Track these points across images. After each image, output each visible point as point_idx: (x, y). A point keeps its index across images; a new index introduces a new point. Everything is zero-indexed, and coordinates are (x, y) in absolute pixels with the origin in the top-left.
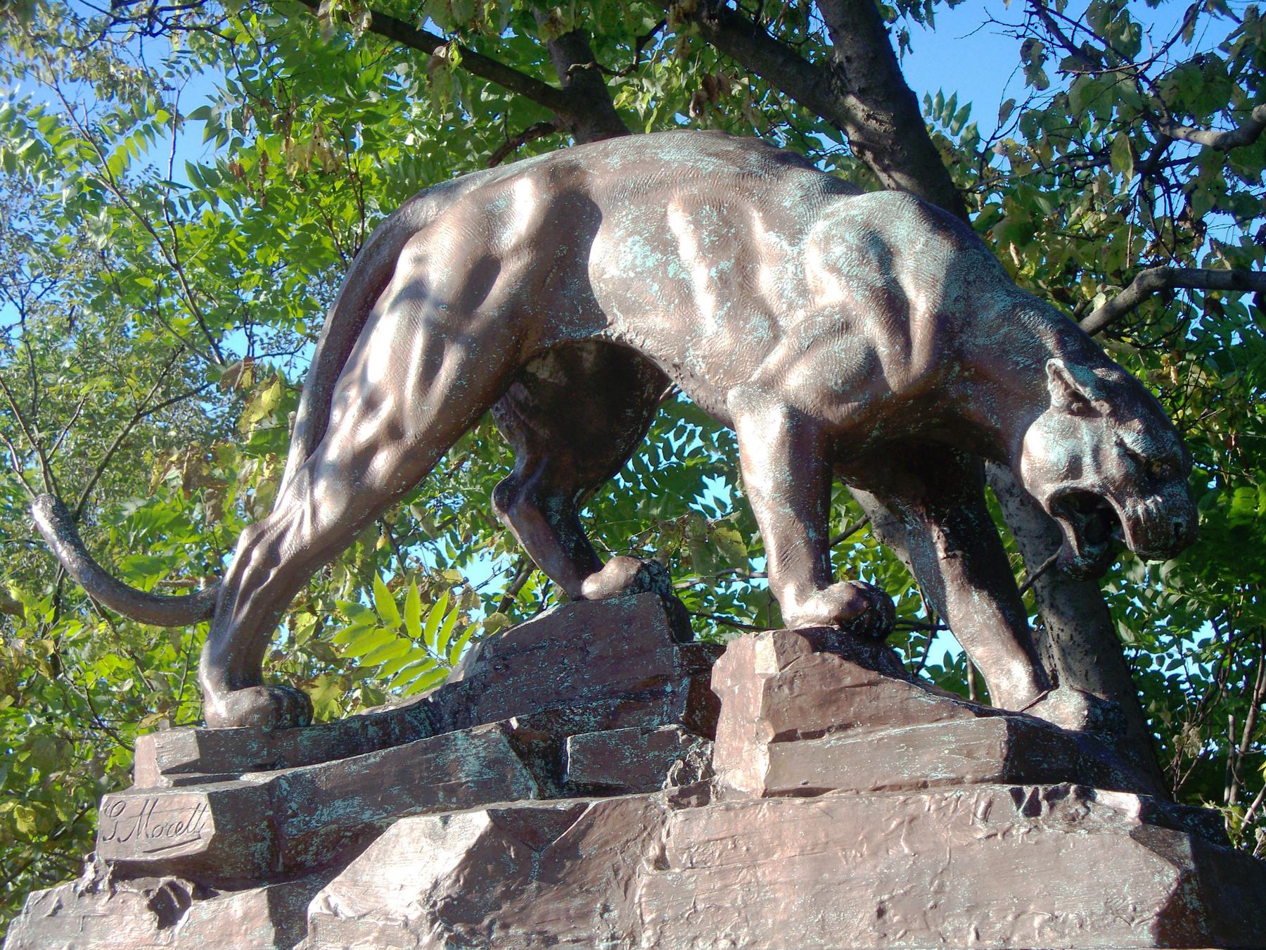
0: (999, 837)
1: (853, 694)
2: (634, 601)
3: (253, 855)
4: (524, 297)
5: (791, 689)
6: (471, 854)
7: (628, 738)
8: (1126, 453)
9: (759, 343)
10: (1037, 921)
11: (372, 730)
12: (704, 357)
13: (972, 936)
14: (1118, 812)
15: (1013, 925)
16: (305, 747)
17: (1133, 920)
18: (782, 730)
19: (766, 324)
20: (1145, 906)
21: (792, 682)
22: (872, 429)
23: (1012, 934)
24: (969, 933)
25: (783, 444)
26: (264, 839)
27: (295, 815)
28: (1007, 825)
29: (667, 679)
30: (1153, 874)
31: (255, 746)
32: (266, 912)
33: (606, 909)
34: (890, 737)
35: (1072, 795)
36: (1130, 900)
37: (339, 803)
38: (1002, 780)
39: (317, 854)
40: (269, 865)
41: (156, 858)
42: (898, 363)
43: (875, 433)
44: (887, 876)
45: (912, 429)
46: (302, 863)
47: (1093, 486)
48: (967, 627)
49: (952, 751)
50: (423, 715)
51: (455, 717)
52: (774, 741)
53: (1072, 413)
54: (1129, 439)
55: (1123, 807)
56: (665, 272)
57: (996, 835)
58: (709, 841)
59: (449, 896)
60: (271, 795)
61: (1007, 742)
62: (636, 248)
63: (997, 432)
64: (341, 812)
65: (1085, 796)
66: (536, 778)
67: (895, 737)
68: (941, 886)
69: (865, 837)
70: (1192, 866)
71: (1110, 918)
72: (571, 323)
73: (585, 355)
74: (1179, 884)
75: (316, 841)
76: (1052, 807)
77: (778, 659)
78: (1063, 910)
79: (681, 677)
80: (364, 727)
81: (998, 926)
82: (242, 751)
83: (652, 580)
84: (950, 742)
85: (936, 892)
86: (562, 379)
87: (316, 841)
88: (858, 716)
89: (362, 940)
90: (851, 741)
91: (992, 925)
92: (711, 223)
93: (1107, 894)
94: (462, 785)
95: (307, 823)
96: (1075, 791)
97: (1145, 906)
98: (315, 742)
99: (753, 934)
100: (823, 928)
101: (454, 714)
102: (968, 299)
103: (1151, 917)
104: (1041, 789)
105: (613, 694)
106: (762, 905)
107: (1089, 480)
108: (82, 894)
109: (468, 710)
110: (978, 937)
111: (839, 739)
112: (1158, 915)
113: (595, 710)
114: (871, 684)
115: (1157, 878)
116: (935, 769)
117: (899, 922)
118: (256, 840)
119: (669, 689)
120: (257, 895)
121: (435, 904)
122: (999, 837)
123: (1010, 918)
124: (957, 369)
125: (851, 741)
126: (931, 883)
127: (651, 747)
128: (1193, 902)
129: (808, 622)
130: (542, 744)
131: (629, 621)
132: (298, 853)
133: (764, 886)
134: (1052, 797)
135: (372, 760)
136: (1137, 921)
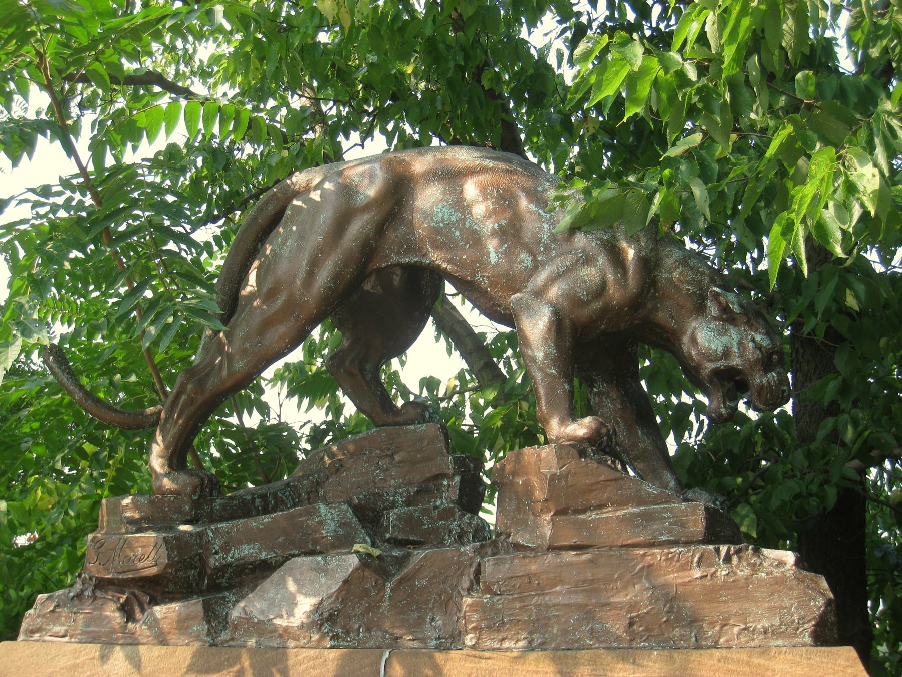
0: (709, 577)
1: (606, 486)
2: (424, 428)
3: (189, 578)
4: (371, 235)
5: (566, 482)
6: (346, 582)
7: (425, 512)
8: (758, 347)
9: (525, 270)
10: (736, 630)
11: (258, 501)
12: (488, 277)
13: (693, 639)
14: (781, 563)
15: (720, 632)
16: (218, 510)
17: (798, 629)
18: (560, 507)
19: (530, 259)
20: (805, 620)
21: (567, 477)
22: (602, 324)
23: (719, 638)
24: (691, 637)
25: (549, 330)
26: (196, 568)
27: (217, 553)
28: (713, 570)
29: (443, 476)
30: (810, 601)
31: (187, 508)
32: (202, 614)
33: (433, 620)
34: (630, 513)
35: (750, 551)
36: (796, 617)
37: (245, 546)
38: (706, 541)
39: (229, 578)
40: (197, 584)
41: (125, 577)
42: (620, 284)
43: (603, 327)
44: (635, 602)
45: (623, 326)
46: (219, 584)
47: (737, 365)
48: (633, 451)
49: (671, 523)
50: (287, 494)
51: (309, 495)
52: (554, 515)
53: (723, 321)
54: (758, 337)
55: (784, 559)
56: (464, 224)
57: (706, 576)
58: (512, 577)
59: (332, 609)
60: (201, 539)
61: (706, 518)
62: (444, 209)
63: (675, 330)
64: (246, 552)
65: (756, 551)
66: (369, 535)
67: (634, 513)
68: (671, 608)
69: (618, 577)
70: (832, 596)
71: (784, 628)
72: (398, 253)
73: (395, 277)
74: (826, 607)
75: (230, 570)
76: (740, 558)
77: (558, 462)
78: (753, 622)
79: (454, 475)
80: (253, 499)
81: (710, 633)
82: (179, 510)
83: (430, 417)
84: (669, 518)
85: (668, 612)
86: (379, 290)
87: (230, 570)
88: (608, 500)
89: (269, 635)
90: (604, 515)
91: (705, 632)
92: (493, 197)
93: (780, 613)
94: (323, 537)
95: (224, 559)
96: (752, 549)
97: (805, 620)
98: (224, 507)
99: (544, 638)
100: (592, 634)
101: (308, 494)
102: (657, 250)
103: (809, 626)
104: (732, 548)
105: (410, 484)
106: (549, 619)
107: (736, 361)
108: (73, 598)
109: (317, 491)
110: (696, 640)
111: (597, 514)
112: (814, 626)
113: (401, 494)
114: (616, 480)
115: (812, 604)
116: (662, 534)
117: (643, 631)
118: (192, 569)
119: (445, 483)
120: (195, 604)
121: (321, 614)
122: (709, 577)
123: (717, 628)
124: (653, 291)
125: (604, 515)
126: (665, 606)
127: (440, 519)
128: (832, 619)
129: (568, 440)
130: (371, 514)
131: (421, 440)
132: (218, 578)
133: (550, 607)
134: (737, 552)
135: (266, 520)
136: (801, 630)
